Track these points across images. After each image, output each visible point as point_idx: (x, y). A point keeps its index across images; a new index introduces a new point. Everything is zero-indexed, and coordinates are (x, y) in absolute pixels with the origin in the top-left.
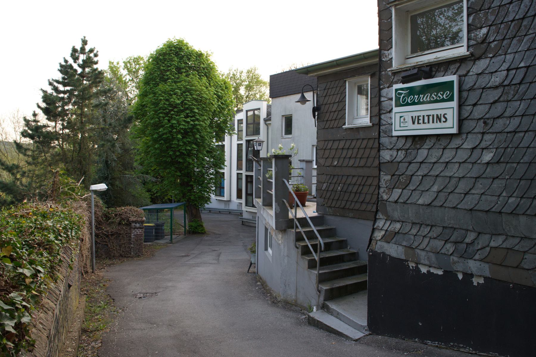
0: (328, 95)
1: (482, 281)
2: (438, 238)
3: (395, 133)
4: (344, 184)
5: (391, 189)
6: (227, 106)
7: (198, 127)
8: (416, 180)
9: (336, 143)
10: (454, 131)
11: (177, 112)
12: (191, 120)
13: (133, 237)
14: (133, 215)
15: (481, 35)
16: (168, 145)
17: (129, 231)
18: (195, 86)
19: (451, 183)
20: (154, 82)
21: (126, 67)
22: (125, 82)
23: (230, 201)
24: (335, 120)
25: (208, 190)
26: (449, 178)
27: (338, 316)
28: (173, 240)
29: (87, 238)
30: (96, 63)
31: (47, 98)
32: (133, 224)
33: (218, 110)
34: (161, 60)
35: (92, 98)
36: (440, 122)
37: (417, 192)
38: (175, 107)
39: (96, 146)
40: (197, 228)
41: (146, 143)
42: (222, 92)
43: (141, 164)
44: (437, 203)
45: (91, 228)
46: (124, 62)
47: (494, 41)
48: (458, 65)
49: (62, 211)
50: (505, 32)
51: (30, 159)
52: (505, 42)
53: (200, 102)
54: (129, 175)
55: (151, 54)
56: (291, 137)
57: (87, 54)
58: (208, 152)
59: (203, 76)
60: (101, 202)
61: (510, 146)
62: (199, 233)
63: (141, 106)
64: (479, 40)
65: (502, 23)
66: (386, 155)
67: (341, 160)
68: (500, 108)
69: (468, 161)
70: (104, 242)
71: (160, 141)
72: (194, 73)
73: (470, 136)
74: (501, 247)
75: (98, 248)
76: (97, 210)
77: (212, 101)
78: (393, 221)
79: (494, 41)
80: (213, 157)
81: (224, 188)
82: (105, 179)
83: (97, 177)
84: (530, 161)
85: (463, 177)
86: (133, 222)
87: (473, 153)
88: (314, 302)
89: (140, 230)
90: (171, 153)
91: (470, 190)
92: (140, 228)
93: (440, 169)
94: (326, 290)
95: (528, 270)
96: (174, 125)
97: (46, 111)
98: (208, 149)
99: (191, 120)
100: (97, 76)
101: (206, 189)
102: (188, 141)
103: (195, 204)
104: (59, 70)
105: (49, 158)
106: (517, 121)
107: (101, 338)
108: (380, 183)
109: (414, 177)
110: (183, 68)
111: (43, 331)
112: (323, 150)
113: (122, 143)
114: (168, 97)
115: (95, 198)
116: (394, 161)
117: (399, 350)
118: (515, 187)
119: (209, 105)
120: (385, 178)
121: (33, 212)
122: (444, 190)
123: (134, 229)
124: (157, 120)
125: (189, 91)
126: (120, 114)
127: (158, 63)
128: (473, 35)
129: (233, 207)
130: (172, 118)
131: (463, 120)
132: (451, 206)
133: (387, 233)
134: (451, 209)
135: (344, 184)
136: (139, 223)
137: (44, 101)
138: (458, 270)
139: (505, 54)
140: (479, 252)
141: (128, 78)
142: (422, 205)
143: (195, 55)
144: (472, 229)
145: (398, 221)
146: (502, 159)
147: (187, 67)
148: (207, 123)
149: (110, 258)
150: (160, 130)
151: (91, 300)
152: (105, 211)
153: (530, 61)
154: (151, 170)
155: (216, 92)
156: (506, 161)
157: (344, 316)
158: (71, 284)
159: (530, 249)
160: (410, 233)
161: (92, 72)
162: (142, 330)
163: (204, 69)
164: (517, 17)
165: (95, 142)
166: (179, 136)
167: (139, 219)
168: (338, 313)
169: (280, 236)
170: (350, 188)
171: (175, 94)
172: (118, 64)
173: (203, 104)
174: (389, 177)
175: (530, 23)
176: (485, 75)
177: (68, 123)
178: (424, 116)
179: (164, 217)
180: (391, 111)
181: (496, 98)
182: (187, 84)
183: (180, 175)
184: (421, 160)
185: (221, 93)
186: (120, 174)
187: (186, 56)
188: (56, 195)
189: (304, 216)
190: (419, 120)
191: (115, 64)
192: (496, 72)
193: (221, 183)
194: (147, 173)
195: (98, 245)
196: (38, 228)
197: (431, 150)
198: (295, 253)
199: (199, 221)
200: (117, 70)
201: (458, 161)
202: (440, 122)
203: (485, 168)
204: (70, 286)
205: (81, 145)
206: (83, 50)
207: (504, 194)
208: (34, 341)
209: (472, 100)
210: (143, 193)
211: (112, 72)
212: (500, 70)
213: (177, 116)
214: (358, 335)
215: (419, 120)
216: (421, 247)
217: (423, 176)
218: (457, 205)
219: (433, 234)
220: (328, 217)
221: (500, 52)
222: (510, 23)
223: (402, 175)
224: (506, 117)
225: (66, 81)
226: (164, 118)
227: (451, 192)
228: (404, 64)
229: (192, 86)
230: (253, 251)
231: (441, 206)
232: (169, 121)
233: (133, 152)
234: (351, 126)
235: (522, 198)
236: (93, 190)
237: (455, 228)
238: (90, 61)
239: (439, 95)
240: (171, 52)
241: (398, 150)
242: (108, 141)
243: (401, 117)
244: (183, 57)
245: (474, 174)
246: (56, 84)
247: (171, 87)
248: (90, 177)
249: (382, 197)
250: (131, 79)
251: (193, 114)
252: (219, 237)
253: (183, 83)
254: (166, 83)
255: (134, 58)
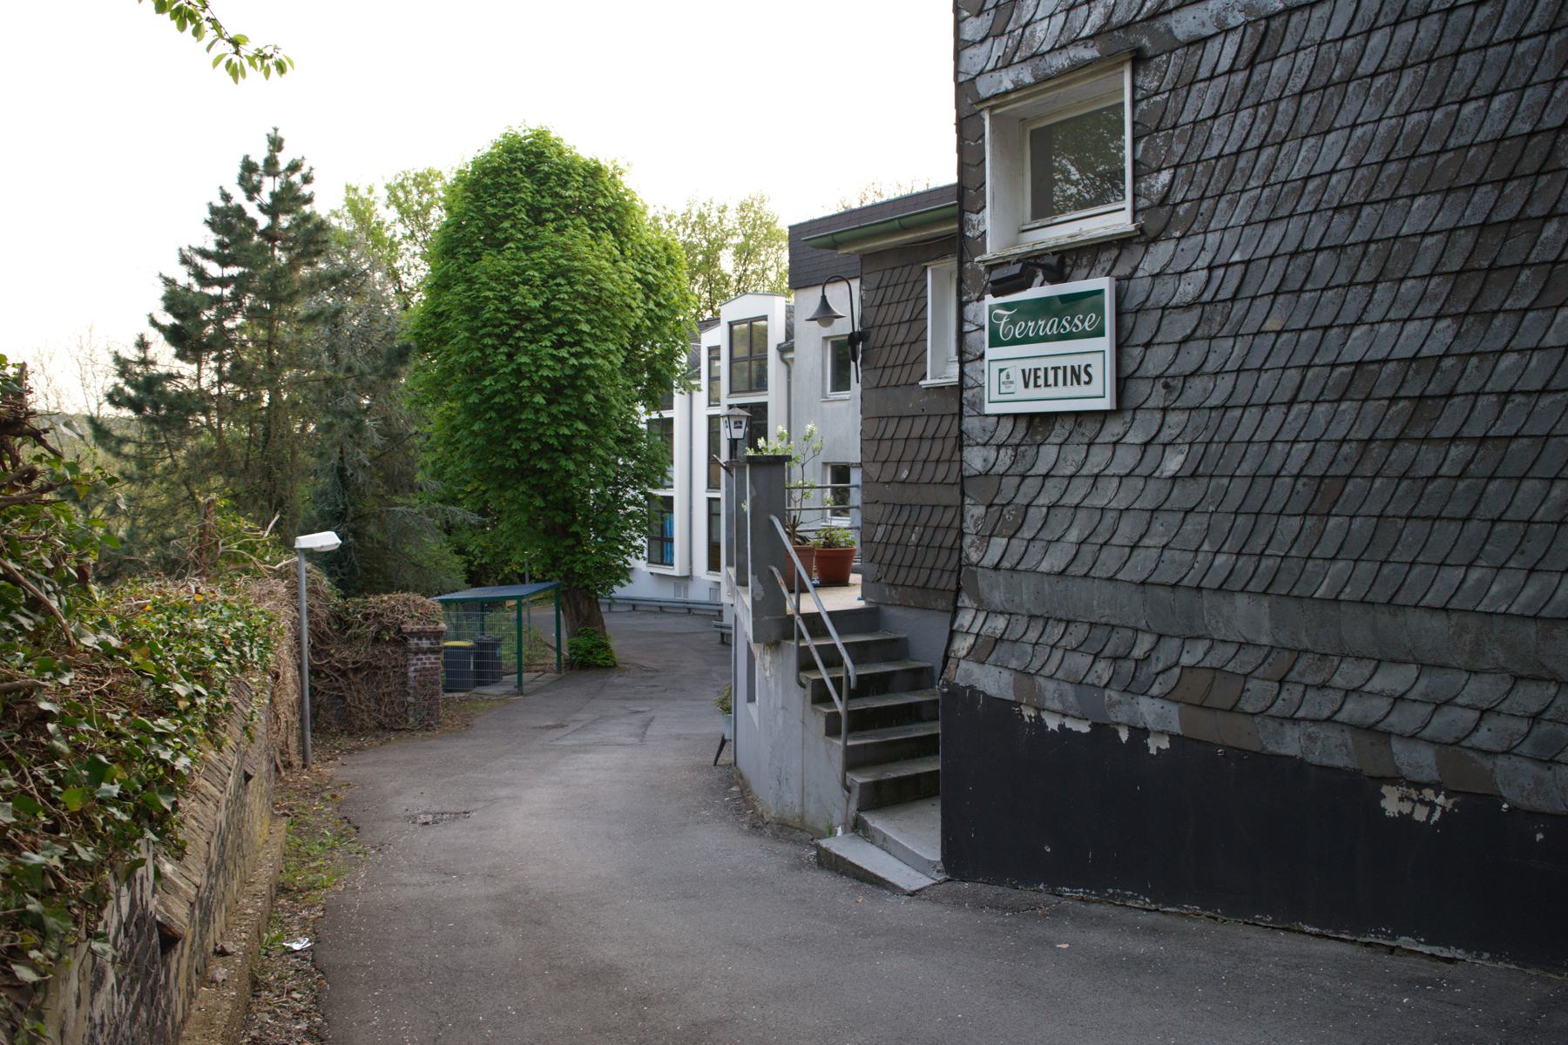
0: (885, 302)
1: (1165, 744)
2: (1082, 649)
3: (989, 409)
4: (925, 526)
5: (986, 538)
6: (674, 313)
7: (591, 372)
8: (1036, 515)
9: (906, 424)
10: (1106, 404)
11: (531, 331)
12: (572, 355)
13: (411, 675)
14: (412, 617)
15: (1159, 186)
16: (508, 422)
17: (401, 661)
18: (582, 260)
19: (1104, 522)
20: (467, 250)
21: (393, 200)
22: (392, 243)
23: (689, 578)
24: (903, 365)
25: (621, 547)
26: (1099, 512)
27: (884, 844)
28: (525, 687)
29: (289, 674)
30: (309, 200)
31: (175, 300)
32: (413, 642)
33: (648, 323)
34: (486, 188)
35: (298, 298)
36: (1079, 383)
37: (1039, 545)
38: (528, 319)
39: (312, 427)
40: (590, 653)
41: (450, 419)
42: (659, 274)
43: (438, 475)
44: (1078, 569)
45: (300, 653)
46: (388, 187)
47: (1183, 201)
48: (1114, 253)
49: (225, 601)
50: (1205, 181)
51: (132, 467)
52: (1206, 204)
53: (596, 304)
54: (408, 506)
55: (460, 171)
56: (847, 397)
57: (283, 176)
58: (619, 441)
59: (603, 230)
60: (325, 581)
61: (1216, 439)
62: (599, 666)
63: (435, 322)
64: (1156, 199)
65: (1198, 161)
66: (976, 459)
67: (918, 467)
68: (1195, 352)
69: (1137, 471)
70: (334, 689)
71: (486, 411)
72: (578, 221)
73: (1139, 415)
74: (1201, 665)
75: (319, 706)
76: (316, 603)
77: (629, 301)
78: (992, 612)
79: (1183, 201)
80: (634, 457)
81: (671, 540)
82: (338, 519)
83: (314, 513)
84: (1251, 473)
85: (1127, 509)
86: (413, 634)
87: (1146, 455)
88: (838, 817)
89: (433, 657)
90: (517, 445)
91: (1141, 537)
92: (433, 651)
93: (1083, 492)
94: (862, 785)
95: (1253, 715)
96: (524, 369)
97: (174, 336)
98: (621, 434)
99: (572, 355)
100: (313, 237)
101: (615, 542)
102: (563, 412)
103: (587, 587)
104: (206, 221)
105: (182, 464)
106: (1226, 383)
107: (324, 901)
108: (965, 525)
109: (1032, 510)
110: (548, 210)
111: (199, 831)
112: (876, 443)
113: (385, 419)
114: (507, 290)
115: (308, 572)
116: (992, 472)
117: (997, 908)
118: (1227, 530)
119: (622, 310)
120: (975, 511)
121: (154, 604)
122: (1091, 540)
123: (416, 653)
124: (476, 354)
125: (564, 272)
126: (376, 338)
127: (478, 198)
128: (1143, 185)
129: (698, 593)
130: (517, 348)
131: (1126, 378)
132: (1105, 576)
133: (980, 641)
134: (1104, 583)
135: (925, 526)
136: (428, 639)
137: (168, 309)
138: (1119, 720)
139: (1205, 233)
140: (1160, 678)
141: (400, 230)
142: (1049, 574)
143: (581, 170)
144: (1145, 628)
145: (1002, 613)
146: (1201, 469)
147: (558, 205)
148: (615, 361)
149: (351, 734)
150: (487, 383)
151: (298, 826)
152: (336, 605)
153: (1251, 250)
154: (462, 491)
155: (639, 275)
156: (1208, 473)
157: (896, 842)
158: (250, 771)
159: (1257, 668)
160: (1024, 639)
161: (298, 226)
162: (422, 886)
163: (607, 209)
164: (1226, 151)
165: (308, 417)
166: (539, 399)
167: (430, 627)
168: (885, 838)
169: (768, 658)
170: (939, 537)
171: (525, 282)
172: (370, 191)
173: (604, 307)
174: (980, 511)
175: (1251, 164)
176: (1166, 277)
177: (234, 367)
178: (1046, 369)
179: (501, 624)
180: (982, 357)
181: (1189, 331)
182: (559, 253)
183: (543, 505)
184: (1044, 471)
185: (655, 276)
186: (380, 506)
187: (557, 175)
188: (209, 561)
189: (816, 610)
190: (1036, 377)
191: (363, 192)
192: (1187, 271)
193: (662, 528)
194: (455, 501)
195: (318, 698)
196: (176, 634)
197: (1064, 447)
198: (799, 699)
199: (596, 632)
200: (367, 209)
201: (1116, 472)
202: (1079, 383)
203: (1169, 487)
204: (248, 777)
205: (270, 425)
206: (271, 166)
207: (1206, 547)
208: (184, 842)
209: (1142, 336)
210: (444, 558)
211: (354, 216)
212: (1194, 267)
213: (531, 342)
214: (920, 881)
215: (1036, 377)
216: (1048, 670)
217: (1049, 508)
218: (1116, 573)
219: (1071, 640)
220: (891, 612)
221: (1195, 227)
222: (1213, 162)
223: (1008, 504)
224: (1208, 374)
225: (227, 252)
226: (495, 348)
227: (1105, 543)
228: (1016, 244)
229: (575, 259)
230: (727, 708)
231: (1086, 576)
232: (510, 356)
233: (417, 441)
234: (937, 381)
235: (1239, 554)
236: (303, 550)
237: (1113, 626)
238: (291, 195)
239: (1076, 321)
240: (513, 166)
241: (999, 447)
242: (344, 414)
243: (1001, 371)
244: (547, 176)
245: (1148, 502)
246: (199, 260)
247: (515, 263)
248: (294, 515)
249: (967, 557)
250: (408, 233)
251: (577, 338)
252: (653, 677)
253: (548, 250)
254: (500, 252)
255: (417, 175)
